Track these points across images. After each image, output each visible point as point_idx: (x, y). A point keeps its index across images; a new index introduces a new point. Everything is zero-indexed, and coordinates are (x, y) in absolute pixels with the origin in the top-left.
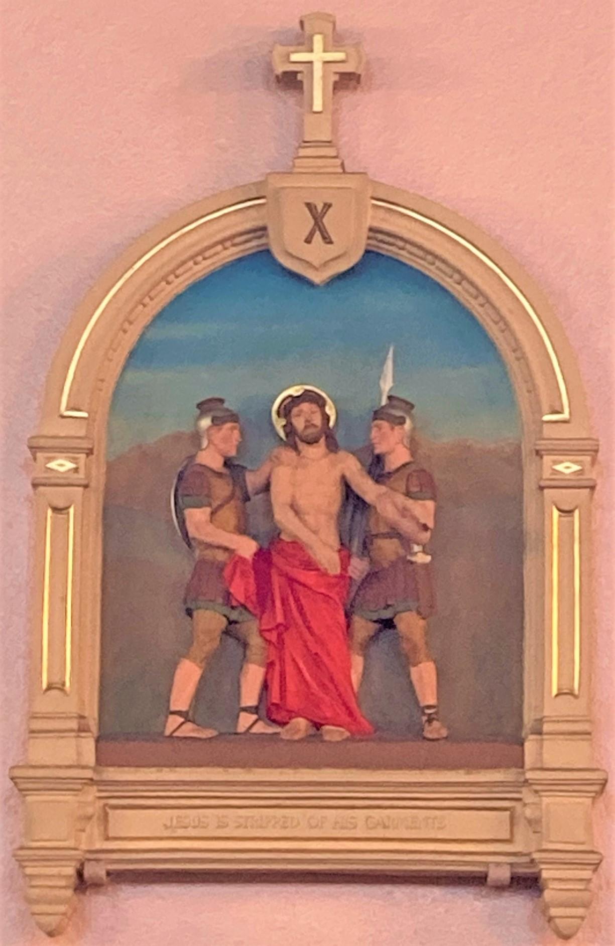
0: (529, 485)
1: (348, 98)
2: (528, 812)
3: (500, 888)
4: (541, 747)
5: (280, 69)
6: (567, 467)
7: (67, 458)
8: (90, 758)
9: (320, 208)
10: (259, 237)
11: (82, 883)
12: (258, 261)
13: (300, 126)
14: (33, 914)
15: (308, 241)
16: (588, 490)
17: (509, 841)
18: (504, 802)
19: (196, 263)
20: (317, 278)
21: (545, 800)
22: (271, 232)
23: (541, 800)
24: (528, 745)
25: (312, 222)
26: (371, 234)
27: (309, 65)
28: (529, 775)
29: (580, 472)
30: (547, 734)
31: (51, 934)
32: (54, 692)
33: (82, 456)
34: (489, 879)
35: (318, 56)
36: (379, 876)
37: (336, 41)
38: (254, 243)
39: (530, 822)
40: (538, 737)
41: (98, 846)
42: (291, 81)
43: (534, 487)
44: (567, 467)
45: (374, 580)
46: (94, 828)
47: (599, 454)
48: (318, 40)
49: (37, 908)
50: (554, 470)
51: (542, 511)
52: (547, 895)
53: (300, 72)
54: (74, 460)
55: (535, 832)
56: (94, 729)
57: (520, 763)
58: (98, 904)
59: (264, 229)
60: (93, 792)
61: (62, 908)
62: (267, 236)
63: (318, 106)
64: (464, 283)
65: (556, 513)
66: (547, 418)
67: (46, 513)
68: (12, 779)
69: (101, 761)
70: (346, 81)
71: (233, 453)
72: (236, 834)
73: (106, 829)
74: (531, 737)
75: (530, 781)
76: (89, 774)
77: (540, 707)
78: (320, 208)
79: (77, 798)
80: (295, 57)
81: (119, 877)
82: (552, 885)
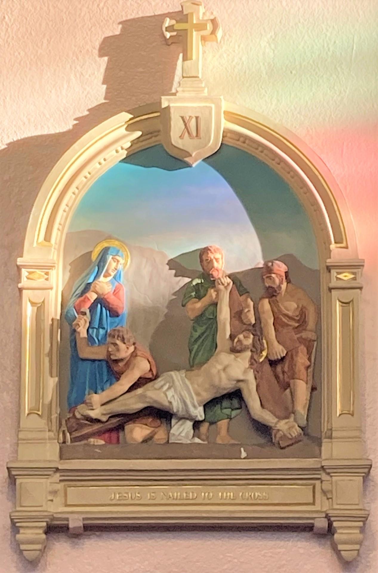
0: (324, 288)
2: (326, 486)
6: (346, 276)
8: (56, 457)
10: (156, 136)
17: (313, 504)
21: (334, 478)
29: (354, 279)
34: (314, 528)
36: (232, 527)
40: (329, 440)
43: (325, 288)
46: (59, 500)
51: (330, 301)
52: (336, 536)
61: (39, 547)
65: (29, 304)
68: (8, 468)
73: (66, 500)
75: (325, 467)
79: (49, 481)
82: (338, 531)
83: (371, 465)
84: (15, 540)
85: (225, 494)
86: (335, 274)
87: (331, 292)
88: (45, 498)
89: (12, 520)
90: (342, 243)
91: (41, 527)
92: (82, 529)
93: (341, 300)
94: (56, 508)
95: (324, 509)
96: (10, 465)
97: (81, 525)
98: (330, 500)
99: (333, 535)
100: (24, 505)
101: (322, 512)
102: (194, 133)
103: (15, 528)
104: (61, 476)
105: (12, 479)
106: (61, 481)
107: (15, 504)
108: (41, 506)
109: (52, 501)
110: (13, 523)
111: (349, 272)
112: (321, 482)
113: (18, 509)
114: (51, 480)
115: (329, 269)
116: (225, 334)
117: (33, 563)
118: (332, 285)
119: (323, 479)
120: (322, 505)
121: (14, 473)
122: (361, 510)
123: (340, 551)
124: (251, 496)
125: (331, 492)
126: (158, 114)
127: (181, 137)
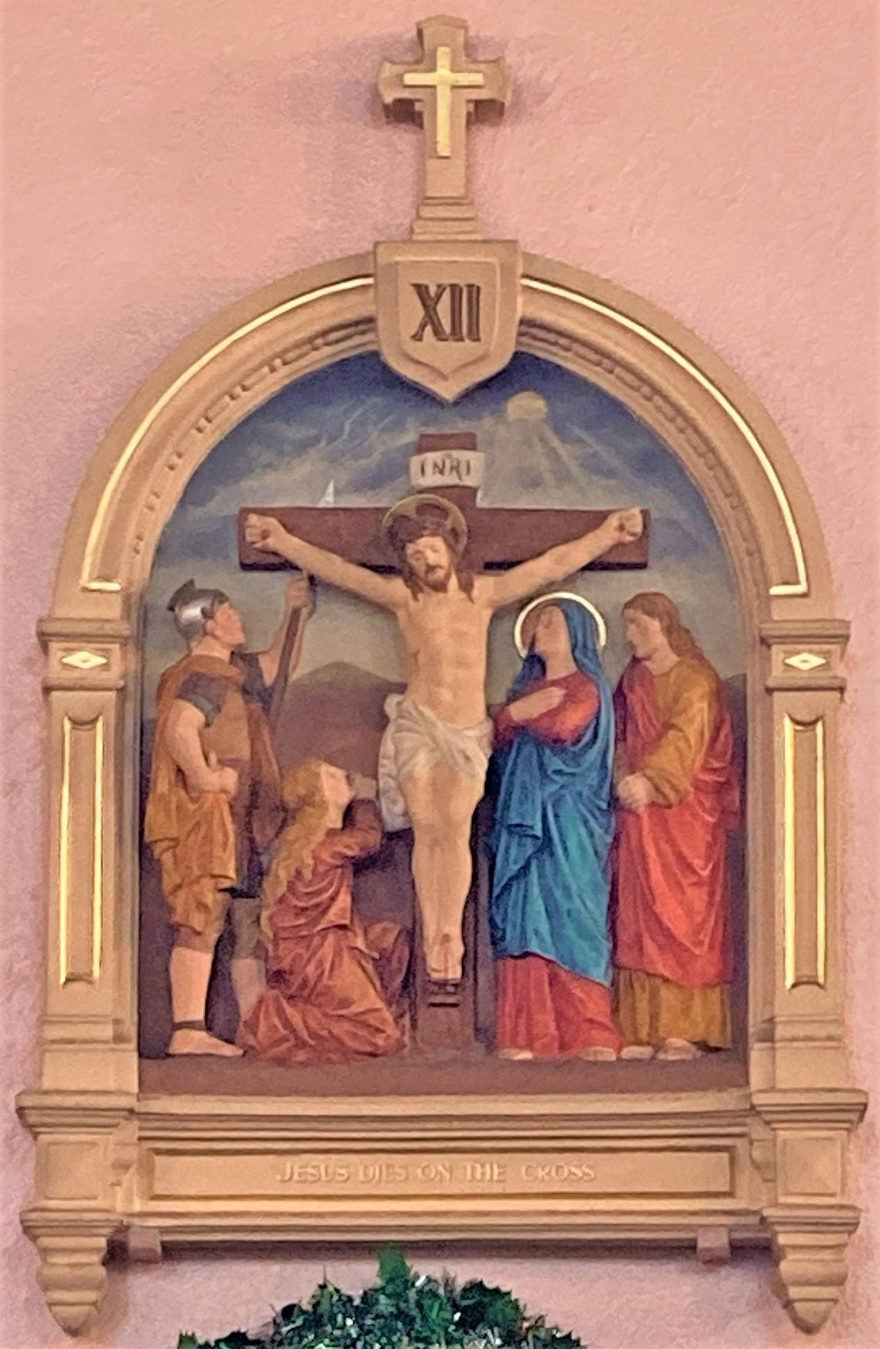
1: (486, 133)
2: (757, 1154)
3: (713, 1262)
4: (774, 1057)
5: (389, 99)
6: (806, 661)
7: (96, 651)
9: (433, 291)
10: (363, 333)
11: (118, 1255)
12: (358, 375)
13: (421, 175)
14: (51, 1305)
15: (418, 337)
17: (729, 1194)
18: (718, 1138)
19: (273, 370)
20: (448, 391)
22: (381, 323)
23: (775, 1137)
25: (421, 313)
26: (524, 329)
27: (429, 90)
28: (759, 1099)
29: (826, 667)
30: (781, 1041)
31: (73, 1332)
32: (77, 987)
33: (115, 647)
35: (443, 75)
37: (469, 52)
39: (757, 1166)
41: (137, 1207)
42: (406, 113)
43: (759, 688)
44: (806, 661)
45: (309, 810)
49: (58, 1295)
50: (787, 665)
52: (784, 1266)
54: (105, 653)
55: (766, 1181)
58: (141, 1286)
59: (371, 320)
60: (132, 1130)
61: (91, 1296)
62: (374, 330)
63: (444, 142)
64: (656, 398)
66: (776, 590)
67: (63, 727)
70: (484, 112)
71: (239, 638)
73: (150, 1187)
76: (124, 1102)
77: (769, 1001)
78: (433, 291)
80: (410, 79)
81: (174, 1252)
83: (865, 1105)
85: (479, 1170)
86: (782, 656)
88: (104, 1184)
90: (797, 582)
91: (98, 1250)
94: (126, 1201)
96: (28, 1101)
98: (770, 1185)
99: (776, 1263)
100: (793, 1190)
102: (447, 327)
104: (141, 1129)
106: (141, 1139)
108: (95, 1198)
111: (811, 652)
112: (751, 1142)
114: (114, 1137)
115: (765, 642)
116: (58, 979)
118: (771, 683)
119: (754, 1136)
122: (842, 1207)
126: (370, 281)
127: (418, 337)
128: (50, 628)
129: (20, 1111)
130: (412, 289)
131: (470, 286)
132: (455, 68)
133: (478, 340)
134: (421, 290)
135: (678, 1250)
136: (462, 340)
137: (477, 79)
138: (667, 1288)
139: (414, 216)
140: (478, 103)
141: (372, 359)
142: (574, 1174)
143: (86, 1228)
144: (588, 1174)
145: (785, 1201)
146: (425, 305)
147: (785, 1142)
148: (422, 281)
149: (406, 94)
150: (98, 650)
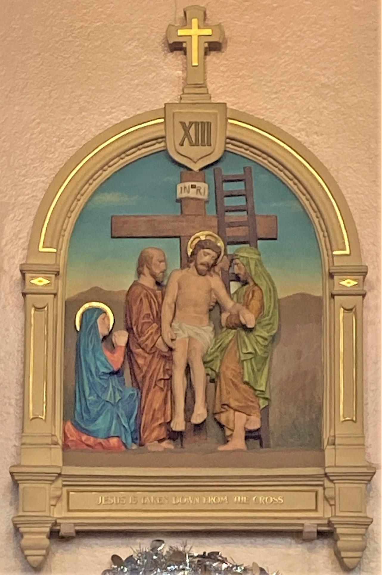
1: (213, 57)
2: (329, 493)
5: (171, 42)
6: (349, 283)
9: (187, 124)
10: (160, 143)
11: (55, 535)
16: (361, 297)
17: (316, 510)
20: (196, 168)
24: (327, 453)
25: (183, 132)
28: (327, 470)
37: (204, 22)
38: (158, 146)
40: (333, 447)
44: (349, 283)
47: (368, 276)
48: (195, 21)
52: (339, 544)
53: (185, 42)
56: (60, 442)
57: (322, 464)
62: (165, 141)
66: (335, 253)
69: (66, 462)
70: (213, 47)
72: (152, 508)
74: (328, 447)
75: (328, 474)
78: (187, 124)
82: (342, 538)
84: (20, 546)
87: (334, 298)
88: (50, 505)
89: (15, 525)
92: (316, 534)
93: (344, 307)
94: (59, 513)
95: (326, 516)
96: (14, 470)
97: (315, 530)
98: (333, 507)
99: (336, 541)
101: (325, 519)
103: (17, 532)
105: (16, 483)
106: (64, 486)
107: (17, 509)
108: (44, 511)
109: (55, 506)
110: (17, 529)
113: (21, 513)
117: (38, 569)
120: (325, 513)
121: (16, 478)
123: (343, 558)
124: (264, 500)
125: (334, 498)
128: (26, 268)
129: (11, 473)
130: (180, 124)
131: (208, 123)
132: (199, 28)
133: (210, 145)
134: (183, 124)
135: (297, 535)
136: (205, 146)
137: (208, 32)
138: (294, 550)
139: (182, 93)
140: (210, 43)
141: (165, 151)
142: (275, 501)
143: (42, 523)
144: (281, 501)
145: (342, 513)
146: (185, 130)
147: (339, 488)
148: (183, 121)
149: (180, 40)
150: (45, 277)
